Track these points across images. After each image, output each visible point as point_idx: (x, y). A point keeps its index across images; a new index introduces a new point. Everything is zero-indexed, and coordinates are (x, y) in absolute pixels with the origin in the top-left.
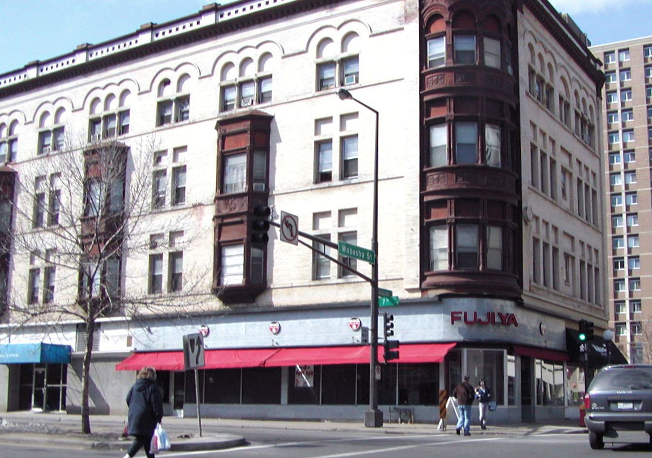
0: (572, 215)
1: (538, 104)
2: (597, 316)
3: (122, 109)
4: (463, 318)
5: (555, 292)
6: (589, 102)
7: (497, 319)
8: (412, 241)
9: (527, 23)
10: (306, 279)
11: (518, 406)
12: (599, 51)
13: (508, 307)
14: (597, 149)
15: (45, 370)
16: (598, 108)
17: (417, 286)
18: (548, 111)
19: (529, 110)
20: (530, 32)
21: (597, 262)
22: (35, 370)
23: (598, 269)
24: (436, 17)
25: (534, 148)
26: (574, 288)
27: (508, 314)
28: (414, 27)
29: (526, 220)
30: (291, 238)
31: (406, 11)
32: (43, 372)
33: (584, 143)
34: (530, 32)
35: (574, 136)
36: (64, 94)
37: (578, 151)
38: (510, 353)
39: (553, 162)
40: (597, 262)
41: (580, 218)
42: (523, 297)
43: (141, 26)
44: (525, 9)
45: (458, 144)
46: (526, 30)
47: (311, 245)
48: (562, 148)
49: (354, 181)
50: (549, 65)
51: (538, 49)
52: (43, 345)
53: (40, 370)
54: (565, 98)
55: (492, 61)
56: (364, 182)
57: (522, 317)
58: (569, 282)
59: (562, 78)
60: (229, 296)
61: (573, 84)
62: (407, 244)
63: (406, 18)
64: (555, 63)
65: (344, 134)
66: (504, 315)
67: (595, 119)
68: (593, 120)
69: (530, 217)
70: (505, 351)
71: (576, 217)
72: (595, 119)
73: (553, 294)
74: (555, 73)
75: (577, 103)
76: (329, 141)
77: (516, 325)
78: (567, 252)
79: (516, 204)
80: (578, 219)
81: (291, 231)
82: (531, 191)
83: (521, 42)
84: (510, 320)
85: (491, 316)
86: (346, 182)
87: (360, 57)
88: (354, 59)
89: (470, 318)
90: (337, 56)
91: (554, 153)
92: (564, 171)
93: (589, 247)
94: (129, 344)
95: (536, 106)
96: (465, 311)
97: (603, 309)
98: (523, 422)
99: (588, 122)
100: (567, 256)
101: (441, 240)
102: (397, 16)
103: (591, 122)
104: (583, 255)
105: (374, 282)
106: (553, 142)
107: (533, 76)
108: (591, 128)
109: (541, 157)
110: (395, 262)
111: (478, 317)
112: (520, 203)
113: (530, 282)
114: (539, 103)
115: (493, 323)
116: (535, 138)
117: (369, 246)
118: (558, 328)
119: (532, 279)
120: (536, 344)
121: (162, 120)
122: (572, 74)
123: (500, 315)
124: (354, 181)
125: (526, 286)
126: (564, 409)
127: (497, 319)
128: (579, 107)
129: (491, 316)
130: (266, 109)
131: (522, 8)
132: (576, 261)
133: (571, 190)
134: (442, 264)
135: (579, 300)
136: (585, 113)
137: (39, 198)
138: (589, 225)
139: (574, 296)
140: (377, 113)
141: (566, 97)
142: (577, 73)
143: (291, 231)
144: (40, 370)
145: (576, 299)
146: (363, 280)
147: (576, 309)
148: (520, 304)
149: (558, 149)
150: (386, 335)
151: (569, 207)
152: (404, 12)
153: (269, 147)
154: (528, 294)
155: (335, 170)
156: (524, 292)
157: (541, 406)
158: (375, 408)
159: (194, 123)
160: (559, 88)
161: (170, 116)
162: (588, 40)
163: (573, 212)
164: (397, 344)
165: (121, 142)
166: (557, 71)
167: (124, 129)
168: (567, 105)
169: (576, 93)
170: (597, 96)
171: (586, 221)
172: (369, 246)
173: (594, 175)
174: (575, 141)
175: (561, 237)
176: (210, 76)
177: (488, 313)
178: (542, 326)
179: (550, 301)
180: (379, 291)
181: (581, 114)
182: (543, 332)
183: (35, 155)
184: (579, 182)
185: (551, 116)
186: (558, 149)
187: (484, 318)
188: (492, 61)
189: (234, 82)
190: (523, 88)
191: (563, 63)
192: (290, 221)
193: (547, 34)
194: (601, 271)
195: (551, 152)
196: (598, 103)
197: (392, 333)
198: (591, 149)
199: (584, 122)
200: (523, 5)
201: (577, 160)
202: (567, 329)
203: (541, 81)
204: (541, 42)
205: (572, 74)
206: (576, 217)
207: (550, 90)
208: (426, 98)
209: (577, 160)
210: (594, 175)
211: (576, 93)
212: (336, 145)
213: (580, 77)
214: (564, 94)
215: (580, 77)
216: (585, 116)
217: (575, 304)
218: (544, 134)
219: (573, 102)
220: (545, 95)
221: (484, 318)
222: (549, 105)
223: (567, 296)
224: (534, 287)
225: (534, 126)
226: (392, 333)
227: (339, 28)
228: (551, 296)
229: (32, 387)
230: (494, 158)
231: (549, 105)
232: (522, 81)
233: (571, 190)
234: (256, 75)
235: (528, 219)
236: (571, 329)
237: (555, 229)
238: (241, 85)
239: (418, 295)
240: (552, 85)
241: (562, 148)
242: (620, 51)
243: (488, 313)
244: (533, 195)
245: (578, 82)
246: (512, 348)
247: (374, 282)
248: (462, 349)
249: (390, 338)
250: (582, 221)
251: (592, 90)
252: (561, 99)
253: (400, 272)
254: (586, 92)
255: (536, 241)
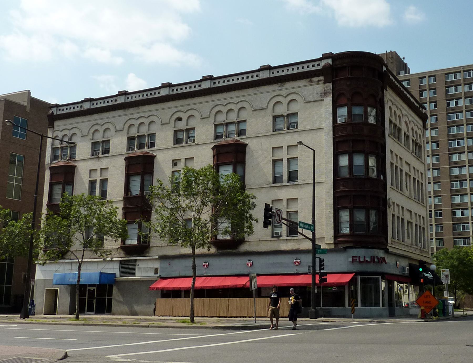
0: (411, 199)
1: (394, 139)
2: (424, 255)
3: (150, 132)
4: (358, 260)
5: (403, 243)
6: (419, 132)
7: (376, 260)
8: (329, 218)
9: (389, 95)
10: (268, 237)
11: (386, 307)
12: (416, 77)
13: (381, 254)
14: (423, 159)
15: (95, 288)
16: (424, 135)
17: (333, 242)
18: (398, 142)
19: (390, 144)
20: (390, 100)
21: (424, 224)
22: (88, 288)
23: (424, 228)
24: (341, 94)
25: (392, 164)
26: (412, 241)
27: (381, 257)
28: (329, 100)
29: (389, 205)
30: (279, 221)
31: (325, 91)
32: (94, 289)
33: (417, 157)
34: (390, 100)
35: (412, 154)
36: (110, 120)
37: (414, 162)
38: (382, 279)
39: (401, 170)
40: (424, 224)
41: (415, 200)
42: (388, 247)
43: (162, 84)
44: (388, 88)
45: (354, 165)
46: (388, 99)
47: (286, 223)
48: (406, 162)
49: (296, 183)
50: (399, 116)
51: (394, 108)
52: (101, 273)
53: (92, 288)
54: (407, 133)
55: (372, 120)
56: (301, 184)
57: (388, 259)
58: (409, 237)
59: (406, 122)
60: (219, 245)
61: (411, 124)
62: (326, 219)
63: (325, 94)
64: (402, 114)
65: (289, 157)
66: (379, 257)
67: (422, 141)
68: (421, 143)
69: (391, 204)
70: (380, 277)
71: (413, 200)
72: (422, 141)
73: (402, 244)
74: (402, 120)
75: (413, 135)
76: (281, 160)
77: (386, 263)
78: (408, 220)
79: (384, 197)
80: (414, 200)
81: (279, 217)
82: (391, 189)
83: (386, 107)
84: (382, 260)
85: (372, 258)
86: (292, 183)
87: (299, 113)
88: (295, 114)
89: (362, 260)
90: (285, 112)
91: (401, 165)
92: (407, 174)
93: (420, 216)
94: (156, 273)
95: (393, 141)
96: (359, 256)
97: (427, 251)
98: (389, 316)
99: (419, 144)
100: (408, 222)
101: (345, 216)
102: (320, 93)
103: (420, 144)
104: (416, 221)
105: (313, 240)
106: (401, 159)
107: (391, 124)
108: (420, 147)
109: (397, 170)
110: (319, 228)
111: (366, 259)
112: (386, 196)
113: (391, 239)
114: (395, 139)
115: (374, 262)
116: (392, 159)
117: (310, 222)
118: (404, 263)
119: (392, 237)
120: (395, 273)
121: (177, 141)
122: (411, 118)
123: (377, 257)
124: (296, 183)
125: (389, 241)
126: (409, 309)
127: (376, 260)
128: (414, 137)
129: (372, 258)
130: (243, 139)
131: (386, 88)
132: (413, 224)
133: (410, 185)
134: (346, 230)
135: (415, 247)
136: (417, 139)
137: (92, 183)
138: (419, 203)
139: (412, 244)
140: (314, 151)
141: (407, 132)
142: (413, 118)
143: (279, 217)
144: (92, 288)
145: (413, 246)
146: (305, 238)
147: (414, 252)
148: (387, 251)
149: (404, 163)
150: (320, 269)
151: (409, 195)
152: (324, 91)
153: (245, 161)
154: (390, 245)
155: (285, 177)
156: (388, 245)
157: (398, 308)
158: (314, 308)
159: (198, 144)
160: (404, 128)
161: (182, 139)
162: (408, 67)
163: (411, 197)
164: (326, 274)
165: (151, 152)
166: (403, 119)
167: (152, 145)
168: (408, 137)
169: (412, 129)
170: (423, 128)
171: (417, 201)
172: (310, 222)
173: (422, 174)
174: (412, 156)
175: (405, 212)
176: (207, 118)
177: (371, 257)
178: (397, 263)
179: (401, 248)
180: (316, 246)
181: (415, 141)
182: (398, 266)
183: (89, 156)
184: (414, 179)
185: (400, 145)
186: (404, 163)
187: (369, 259)
188: (372, 120)
189: (223, 122)
190: (387, 132)
191: (406, 113)
192: (279, 213)
193: (398, 99)
194: (426, 229)
195: (400, 165)
196: (424, 132)
197: (323, 269)
198: (420, 159)
199: (416, 144)
200: (387, 86)
201: (413, 167)
202: (409, 263)
203: (395, 126)
204: (395, 104)
205: (411, 118)
206: (413, 200)
207: (400, 130)
208: (337, 140)
209: (413, 167)
210: (422, 174)
211: (412, 129)
212: (285, 162)
213: (415, 119)
214: (406, 131)
215: (415, 119)
216: (417, 141)
217: (413, 249)
218: (396, 156)
219: (411, 134)
220: (397, 133)
221: (369, 259)
222: (399, 138)
223: (409, 245)
224: (393, 241)
225: (392, 152)
226: (323, 269)
227: (286, 97)
228: (401, 246)
229: (86, 299)
230: (373, 174)
231: (399, 138)
232: (387, 128)
233: (410, 185)
234: (236, 120)
235: (390, 205)
236: (411, 263)
237: (403, 208)
238: (227, 124)
239: (333, 247)
240: (401, 127)
241: (406, 162)
242: (429, 77)
243: (371, 257)
244: (392, 191)
245: (413, 122)
246: (384, 275)
247: (313, 240)
248: (358, 276)
249: (322, 271)
250: (416, 202)
251: (421, 125)
252: (405, 133)
253: (322, 234)
254: (418, 127)
255: (393, 215)
